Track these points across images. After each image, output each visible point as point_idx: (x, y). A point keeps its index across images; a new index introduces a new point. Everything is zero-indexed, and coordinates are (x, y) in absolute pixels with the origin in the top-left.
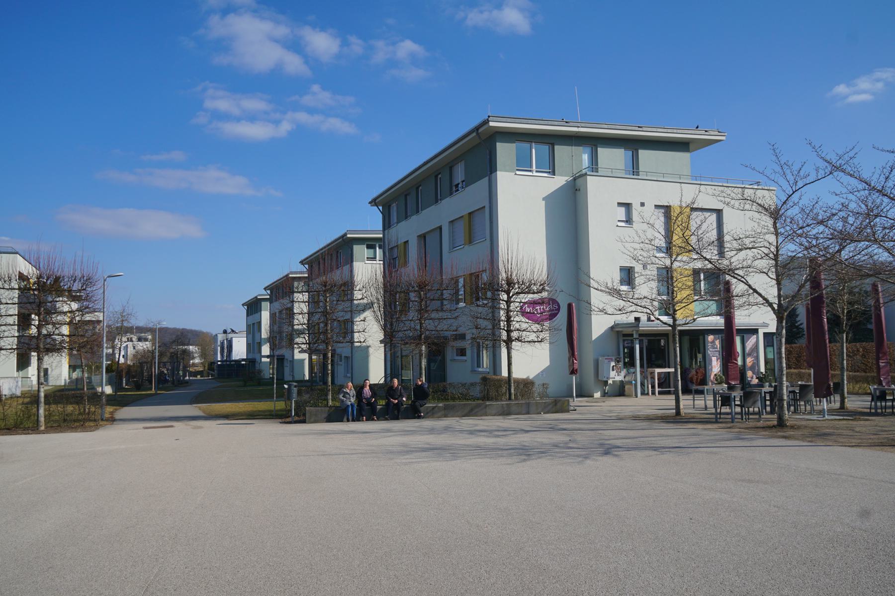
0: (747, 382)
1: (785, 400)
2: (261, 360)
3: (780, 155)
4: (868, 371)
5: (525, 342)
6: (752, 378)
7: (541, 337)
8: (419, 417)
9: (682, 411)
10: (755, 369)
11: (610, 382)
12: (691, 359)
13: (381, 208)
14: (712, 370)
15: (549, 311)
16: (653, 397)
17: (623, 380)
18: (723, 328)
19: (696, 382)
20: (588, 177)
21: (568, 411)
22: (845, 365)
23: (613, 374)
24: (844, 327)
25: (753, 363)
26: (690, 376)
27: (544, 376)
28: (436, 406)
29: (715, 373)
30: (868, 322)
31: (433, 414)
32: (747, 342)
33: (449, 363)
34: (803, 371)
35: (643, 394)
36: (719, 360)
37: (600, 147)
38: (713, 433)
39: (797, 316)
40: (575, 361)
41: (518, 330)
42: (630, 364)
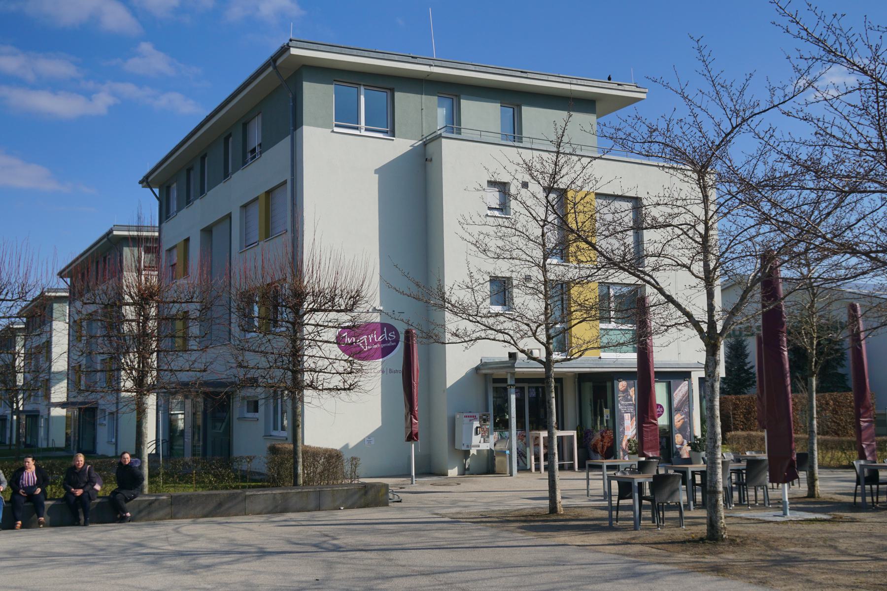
0: (675, 450)
1: (720, 492)
2: (49, 414)
3: (710, 59)
4: (840, 432)
5: (322, 390)
6: (682, 444)
7: (349, 382)
8: (123, 520)
9: (561, 502)
10: (686, 431)
11: (473, 451)
12: (595, 415)
13: (157, 191)
14: (623, 432)
15: (384, 342)
16: (538, 475)
17: (493, 449)
18: (636, 370)
19: (602, 451)
20: (443, 140)
21: (385, 504)
22: (815, 427)
23: (476, 439)
24: (813, 367)
25: (684, 423)
26: (593, 442)
27: (373, 443)
28: (156, 500)
29: (628, 438)
30: (838, 364)
31: (149, 513)
32: (675, 390)
33: (237, 426)
34: (754, 433)
35: (520, 470)
36: (634, 418)
37: (464, 99)
38: (589, 556)
39: (746, 356)
40: (414, 421)
41: (311, 370)
42: (502, 424)
